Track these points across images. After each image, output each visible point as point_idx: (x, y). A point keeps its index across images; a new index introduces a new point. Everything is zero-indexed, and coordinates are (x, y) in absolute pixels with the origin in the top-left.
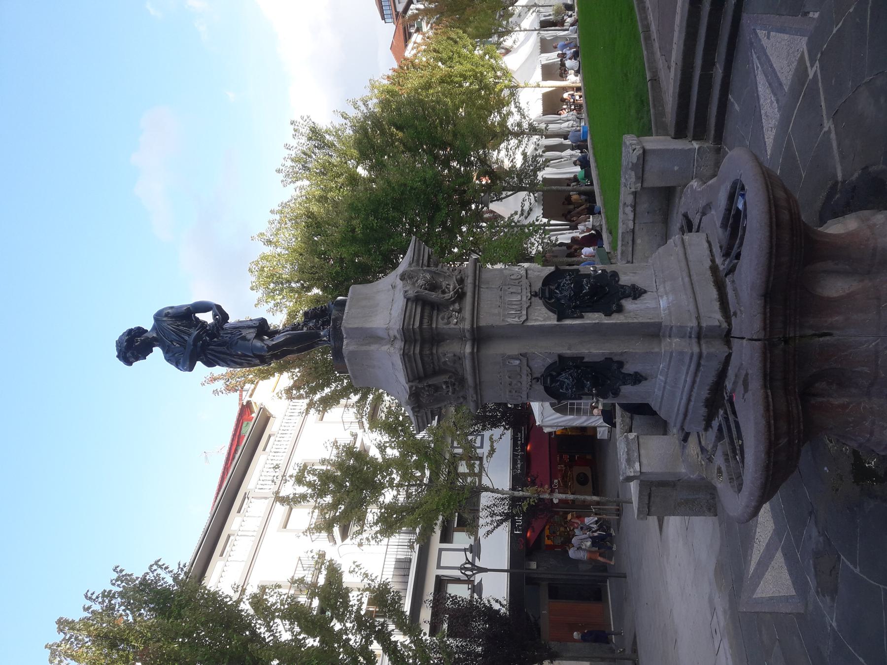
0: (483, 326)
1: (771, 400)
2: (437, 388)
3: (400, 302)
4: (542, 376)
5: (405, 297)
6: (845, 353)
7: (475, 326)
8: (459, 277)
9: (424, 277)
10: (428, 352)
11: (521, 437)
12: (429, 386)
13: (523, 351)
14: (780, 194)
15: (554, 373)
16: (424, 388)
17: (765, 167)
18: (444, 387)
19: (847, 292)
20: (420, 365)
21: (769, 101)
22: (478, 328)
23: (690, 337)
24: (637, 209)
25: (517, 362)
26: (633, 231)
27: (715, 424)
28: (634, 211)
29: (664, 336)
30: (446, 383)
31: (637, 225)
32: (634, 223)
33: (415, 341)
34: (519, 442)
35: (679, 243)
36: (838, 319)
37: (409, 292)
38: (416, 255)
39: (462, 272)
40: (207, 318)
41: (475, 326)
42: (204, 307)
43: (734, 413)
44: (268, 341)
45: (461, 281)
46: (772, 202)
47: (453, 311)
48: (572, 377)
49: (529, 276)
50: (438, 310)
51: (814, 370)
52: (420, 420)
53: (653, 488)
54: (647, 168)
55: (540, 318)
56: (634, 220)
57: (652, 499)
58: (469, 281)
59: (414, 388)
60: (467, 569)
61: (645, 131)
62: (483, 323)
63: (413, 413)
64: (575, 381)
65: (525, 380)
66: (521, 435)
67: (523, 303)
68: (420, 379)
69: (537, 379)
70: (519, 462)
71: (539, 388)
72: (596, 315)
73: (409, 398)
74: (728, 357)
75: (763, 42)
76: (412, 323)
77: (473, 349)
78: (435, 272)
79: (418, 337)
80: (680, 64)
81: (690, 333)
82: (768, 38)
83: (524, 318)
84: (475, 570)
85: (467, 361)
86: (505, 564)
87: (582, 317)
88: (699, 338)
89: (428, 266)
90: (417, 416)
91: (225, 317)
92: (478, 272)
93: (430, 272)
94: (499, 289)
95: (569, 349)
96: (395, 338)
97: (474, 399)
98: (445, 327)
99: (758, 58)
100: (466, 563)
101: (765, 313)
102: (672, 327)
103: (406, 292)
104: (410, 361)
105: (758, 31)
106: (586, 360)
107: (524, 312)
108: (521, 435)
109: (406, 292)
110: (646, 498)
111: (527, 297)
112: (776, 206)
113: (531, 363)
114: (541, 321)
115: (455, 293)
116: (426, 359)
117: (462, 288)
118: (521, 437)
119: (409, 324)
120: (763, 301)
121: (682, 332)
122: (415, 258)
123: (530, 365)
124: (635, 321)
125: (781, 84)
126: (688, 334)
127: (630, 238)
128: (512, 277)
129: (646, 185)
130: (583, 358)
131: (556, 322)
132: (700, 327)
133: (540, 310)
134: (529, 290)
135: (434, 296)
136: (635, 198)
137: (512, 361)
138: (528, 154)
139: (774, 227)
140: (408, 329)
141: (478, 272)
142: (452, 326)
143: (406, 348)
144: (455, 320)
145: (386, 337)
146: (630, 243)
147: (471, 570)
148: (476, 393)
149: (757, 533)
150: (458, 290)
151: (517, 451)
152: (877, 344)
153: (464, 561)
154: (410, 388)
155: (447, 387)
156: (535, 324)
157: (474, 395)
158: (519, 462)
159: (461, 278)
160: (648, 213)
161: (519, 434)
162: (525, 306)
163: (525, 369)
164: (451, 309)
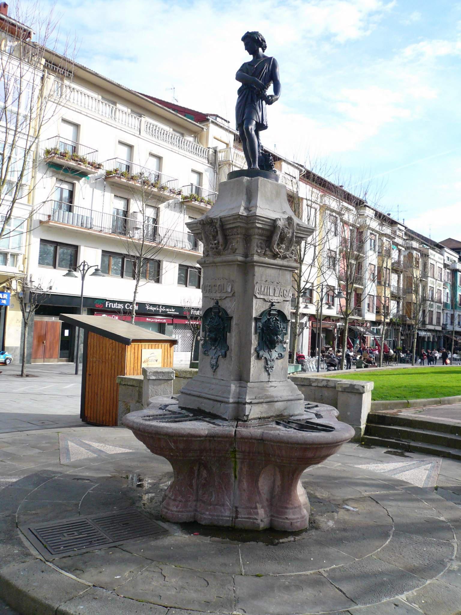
0: (254, 269)
1: (198, 439)
2: (215, 238)
3: (273, 215)
4: (219, 306)
5: (276, 219)
6: (224, 488)
7: (255, 264)
8: (288, 256)
9: (289, 233)
10: (239, 232)
11: (172, 312)
12: (217, 232)
13: (236, 294)
14: (324, 453)
15: (220, 314)
16: (216, 228)
17: (342, 444)
18: (216, 242)
19: (261, 492)
20: (231, 226)
21: (386, 468)
22: (253, 266)
23: (239, 398)
24: (324, 389)
25: (229, 290)
26: (310, 385)
27: (184, 411)
28: (324, 387)
29: (240, 383)
30: (219, 242)
31: (314, 388)
32: (315, 386)
33: (247, 224)
34: (168, 310)
35: (299, 397)
36: (245, 485)
37: (279, 221)
38: (303, 229)
39: (290, 259)
40: (270, 91)
41: (255, 264)
42: (276, 90)
43: (190, 420)
44: (252, 127)
45: (285, 257)
46: (319, 446)
47: (266, 250)
48: (218, 325)
49: (285, 302)
50: (267, 241)
51: (214, 470)
52: (194, 225)
53: (137, 389)
54: (350, 395)
55: (257, 306)
56: (317, 386)
57: (131, 387)
58: (285, 262)
59: (216, 221)
60: (84, 266)
61: (375, 395)
62: (256, 269)
63: (200, 221)
64: (215, 327)
65: (218, 296)
66: (173, 312)
67: (268, 296)
68: (222, 226)
69: (217, 303)
70: (155, 309)
71: (212, 304)
72: (256, 343)
73: (210, 218)
74: (225, 420)
75: (423, 467)
76: (259, 222)
77: (240, 261)
78: (291, 240)
79: (250, 226)
80: (417, 419)
81: (241, 398)
82: (425, 469)
83: (258, 296)
84: (83, 272)
85: (232, 257)
86: (86, 294)
87: (256, 332)
88: (238, 403)
89: (296, 237)
90: (197, 223)
91: (270, 102)
92: (290, 269)
93: (292, 237)
94: (278, 282)
95: (236, 324)
96: (250, 211)
97: (206, 261)
98: (255, 244)
99: (414, 464)
100: (88, 266)
101: (251, 438)
102: (245, 387)
103: (280, 219)
104: (234, 219)
105: (430, 464)
106: (228, 334)
107: (262, 297)
108: (173, 312)
109: (280, 219)
110: (131, 384)
111: (272, 300)
112: (317, 448)
113: (228, 299)
114: (255, 307)
115: (277, 252)
116: (235, 230)
117: (280, 257)
118: (172, 312)
119: (259, 220)
120: (259, 438)
121: (241, 394)
122: (301, 228)
123: (227, 299)
124: (252, 366)
125: (395, 474)
126: (241, 397)
127: (305, 384)
128: (285, 291)
129: (339, 394)
130: (230, 332)
131: (254, 316)
132: (245, 403)
133: (263, 307)
134: (276, 301)
135: (276, 238)
136: (332, 387)
137: (230, 287)
138: (346, 237)
139: (305, 446)
140: (256, 219)
141: (290, 269)
142: (256, 249)
143: (243, 217)
144: (259, 251)
145: (251, 205)
146: (303, 383)
147: (84, 270)
148: (210, 263)
149: (108, 446)
150: (279, 255)
151: (162, 307)
152: (228, 506)
153: (90, 265)
154: (217, 218)
155: (215, 244)
156: (254, 303)
157: (208, 262)
158: (155, 309)
159: (287, 258)
160: (321, 396)
161: (174, 310)
162: (266, 297)
163: (225, 295)
164: (267, 249)
